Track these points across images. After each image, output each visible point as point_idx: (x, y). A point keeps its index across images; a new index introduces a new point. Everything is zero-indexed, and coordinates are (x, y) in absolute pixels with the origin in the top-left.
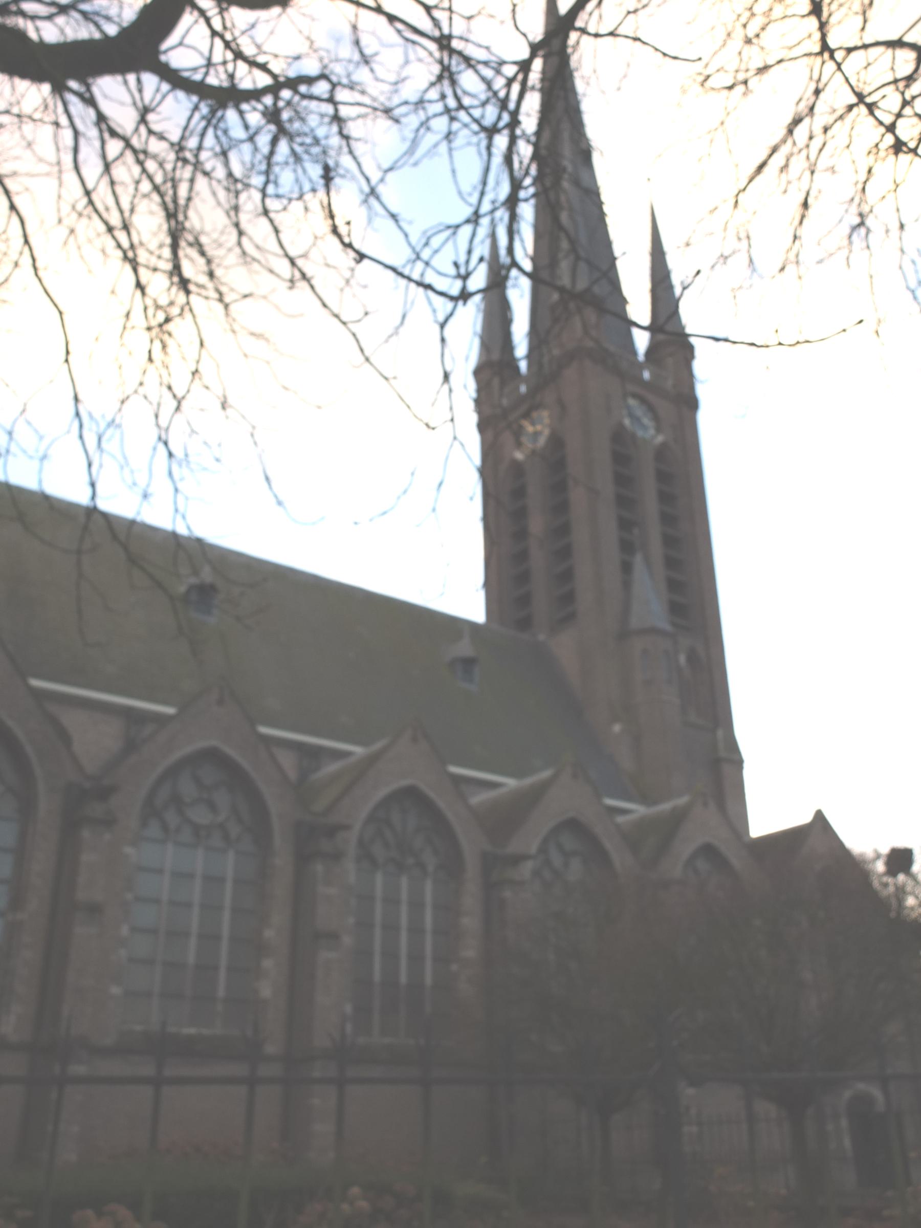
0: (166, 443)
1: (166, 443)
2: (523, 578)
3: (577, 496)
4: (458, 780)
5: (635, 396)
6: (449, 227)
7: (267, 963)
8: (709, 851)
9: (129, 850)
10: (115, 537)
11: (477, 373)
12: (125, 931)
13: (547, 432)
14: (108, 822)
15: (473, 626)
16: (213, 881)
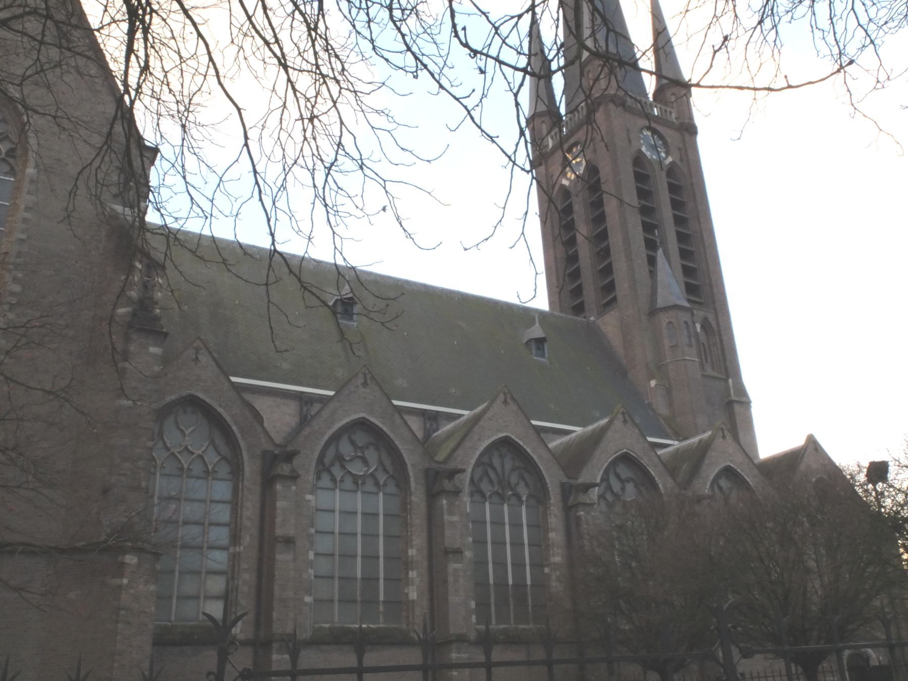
3: (611, 207)
4: (538, 430)
6: (512, 17)
7: (412, 574)
8: (729, 472)
9: (309, 497)
12: (311, 555)
14: (294, 477)
15: (541, 313)
16: (370, 516)
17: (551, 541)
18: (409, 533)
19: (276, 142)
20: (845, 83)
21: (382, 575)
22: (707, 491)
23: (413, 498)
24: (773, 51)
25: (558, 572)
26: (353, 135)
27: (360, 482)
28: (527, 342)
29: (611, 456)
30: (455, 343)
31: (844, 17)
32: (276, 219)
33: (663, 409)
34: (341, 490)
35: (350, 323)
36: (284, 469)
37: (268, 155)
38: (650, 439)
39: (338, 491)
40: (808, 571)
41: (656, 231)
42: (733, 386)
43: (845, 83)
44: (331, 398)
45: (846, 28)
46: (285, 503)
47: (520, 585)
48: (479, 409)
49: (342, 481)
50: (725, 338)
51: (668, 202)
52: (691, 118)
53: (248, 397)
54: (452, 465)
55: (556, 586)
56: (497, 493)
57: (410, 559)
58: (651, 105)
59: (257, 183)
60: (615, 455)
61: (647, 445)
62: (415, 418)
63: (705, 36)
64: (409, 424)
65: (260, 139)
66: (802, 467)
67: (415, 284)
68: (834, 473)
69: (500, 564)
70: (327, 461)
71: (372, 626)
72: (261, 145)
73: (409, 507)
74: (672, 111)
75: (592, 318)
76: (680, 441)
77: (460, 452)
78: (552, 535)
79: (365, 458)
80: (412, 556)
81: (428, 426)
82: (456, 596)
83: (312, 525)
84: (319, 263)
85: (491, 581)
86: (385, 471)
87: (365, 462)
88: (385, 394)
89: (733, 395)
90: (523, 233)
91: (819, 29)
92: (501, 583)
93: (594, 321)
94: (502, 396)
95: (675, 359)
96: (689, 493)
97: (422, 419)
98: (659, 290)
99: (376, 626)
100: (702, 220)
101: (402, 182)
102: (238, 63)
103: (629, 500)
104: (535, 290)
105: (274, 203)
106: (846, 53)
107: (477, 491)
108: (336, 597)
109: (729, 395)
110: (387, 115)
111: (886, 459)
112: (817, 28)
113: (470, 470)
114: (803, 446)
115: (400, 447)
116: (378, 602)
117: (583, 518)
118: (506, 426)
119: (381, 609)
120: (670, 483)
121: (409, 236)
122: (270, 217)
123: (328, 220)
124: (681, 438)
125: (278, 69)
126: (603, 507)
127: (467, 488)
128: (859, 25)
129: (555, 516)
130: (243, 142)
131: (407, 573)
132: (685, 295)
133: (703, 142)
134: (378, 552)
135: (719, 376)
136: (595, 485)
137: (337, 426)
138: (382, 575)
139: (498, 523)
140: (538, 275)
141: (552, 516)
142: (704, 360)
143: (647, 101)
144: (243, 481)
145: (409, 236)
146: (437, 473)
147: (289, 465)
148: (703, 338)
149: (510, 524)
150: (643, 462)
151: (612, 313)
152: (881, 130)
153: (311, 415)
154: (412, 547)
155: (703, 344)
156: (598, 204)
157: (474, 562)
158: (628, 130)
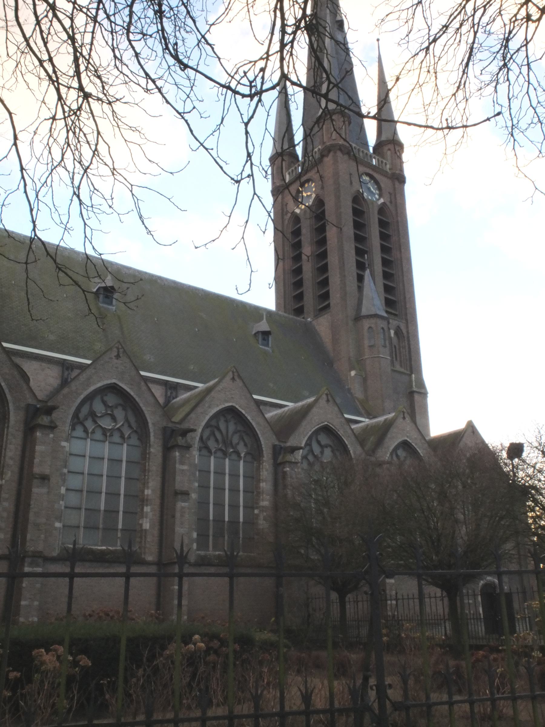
0: (78, 197)
1: (78, 197)
2: (299, 284)
3: (331, 233)
4: (258, 403)
5: (368, 175)
6: (251, 62)
7: (147, 509)
8: (406, 445)
9: (64, 444)
10: (48, 254)
11: (273, 160)
12: (63, 490)
13: (314, 196)
14: (52, 427)
15: (269, 313)
16: (115, 462)
17: (261, 490)
18: (146, 477)
19: (45, 147)
20: (514, 149)
21: (121, 509)
22: (387, 457)
23: (152, 450)
24: (462, 116)
25: (265, 514)
26: (108, 145)
27: (108, 434)
28: (255, 334)
29: (314, 427)
30: (197, 330)
31: (520, 97)
32: (38, 209)
33: (358, 393)
34: (91, 440)
35: (110, 307)
36: (45, 420)
37: (38, 157)
38: (346, 416)
39: (89, 440)
40: (457, 521)
41: (366, 255)
42: (415, 380)
43: (514, 149)
44: (89, 366)
45: (520, 107)
46: (44, 447)
47: (234, 522)
48: (212, 383)
49: (93, 432)
50: (412, 342)
51: (377, 234)
52: (402, 170)
53: (18, 360)
54: (185, 426)
55: (263, 524)
56: (221, 450)
57: (146, 497)
58: (371, 156)
59: (23, 177)
60: (318, 426)
61: (343, 420)
62: (159, 387)
63: (409, 98)
64: (153, 391)
65: (32, 142)
66: (461, 445)
67: (167, 280)
68: (483, 448)
69: (219, 505)
70: (81, 416)
71: (110, 548)
72: (32, 148)
73: (148, 456)
75: (309, 319)
76: (370, 419)
77: (193, 415)
78: (263, 485)
79: (114, 416)
80: (148, 495)
81: (169, 393)
82: (182, 528)
83: (65, 467)
84: (72, 251)
85: (211, 518)
86: (130, 426)
87: (114, 419)
88: (134, 365)
89: (414, 387)
90: (243, 238)
91: (499, 105)
92: (219, 520)
93: (311, 322)
94: (230, 375)
95: (372, 356)
96: (373, 459)
97: (164, 388)
98: (364, 302)
99: (114, 548)
100: (403, 250)
101: (147, 188)
102: (16, 77)
103: (325, 461)
104: (250, 284)
105: (37, 196)
106: (519, 127)
107: (204, 447)
108: (82, 524)
109: (411, 386)
110: (140, 132)
111: (522, 442)
112: (497, 103)
113: (200, 430)
114: (464, 429)
115: (144, 408)
116: (117, 530)
117: (288, 473)
118: (232, 398)
119: (119, 535)
120: (359, 449)
121: (149, 232)
122: (32, 207)
123: (81, 213)
124: (371, 417)
125: (48, 83)
126: (305, 465)
127: (196, 444)
128: (531, 106)
129: (267, 470)
130: (12, 142)
131: (143, 509)
132: (385, 307)
133: (408, 188)
134: (120, 490)
135: (405, 371)
136: (301, 448)
137: (92, 388)
138: (121, 509)
139: (220, 473)
140: (253, 272)
141: (264, 470)
142: (394, 359)
143: (368, 152)
144: (8, 427)
145: (149, 232)
146: (173, 431)
147: (49, 418)
148: (395, 341)
149: (229, 475)
151: (326, 316)
152: (536, 189)
153: (71, 378)
154: (148, 488)
155: (395, 347)
156: (321, 230)
157: (198, 502)
158: (351, 174)
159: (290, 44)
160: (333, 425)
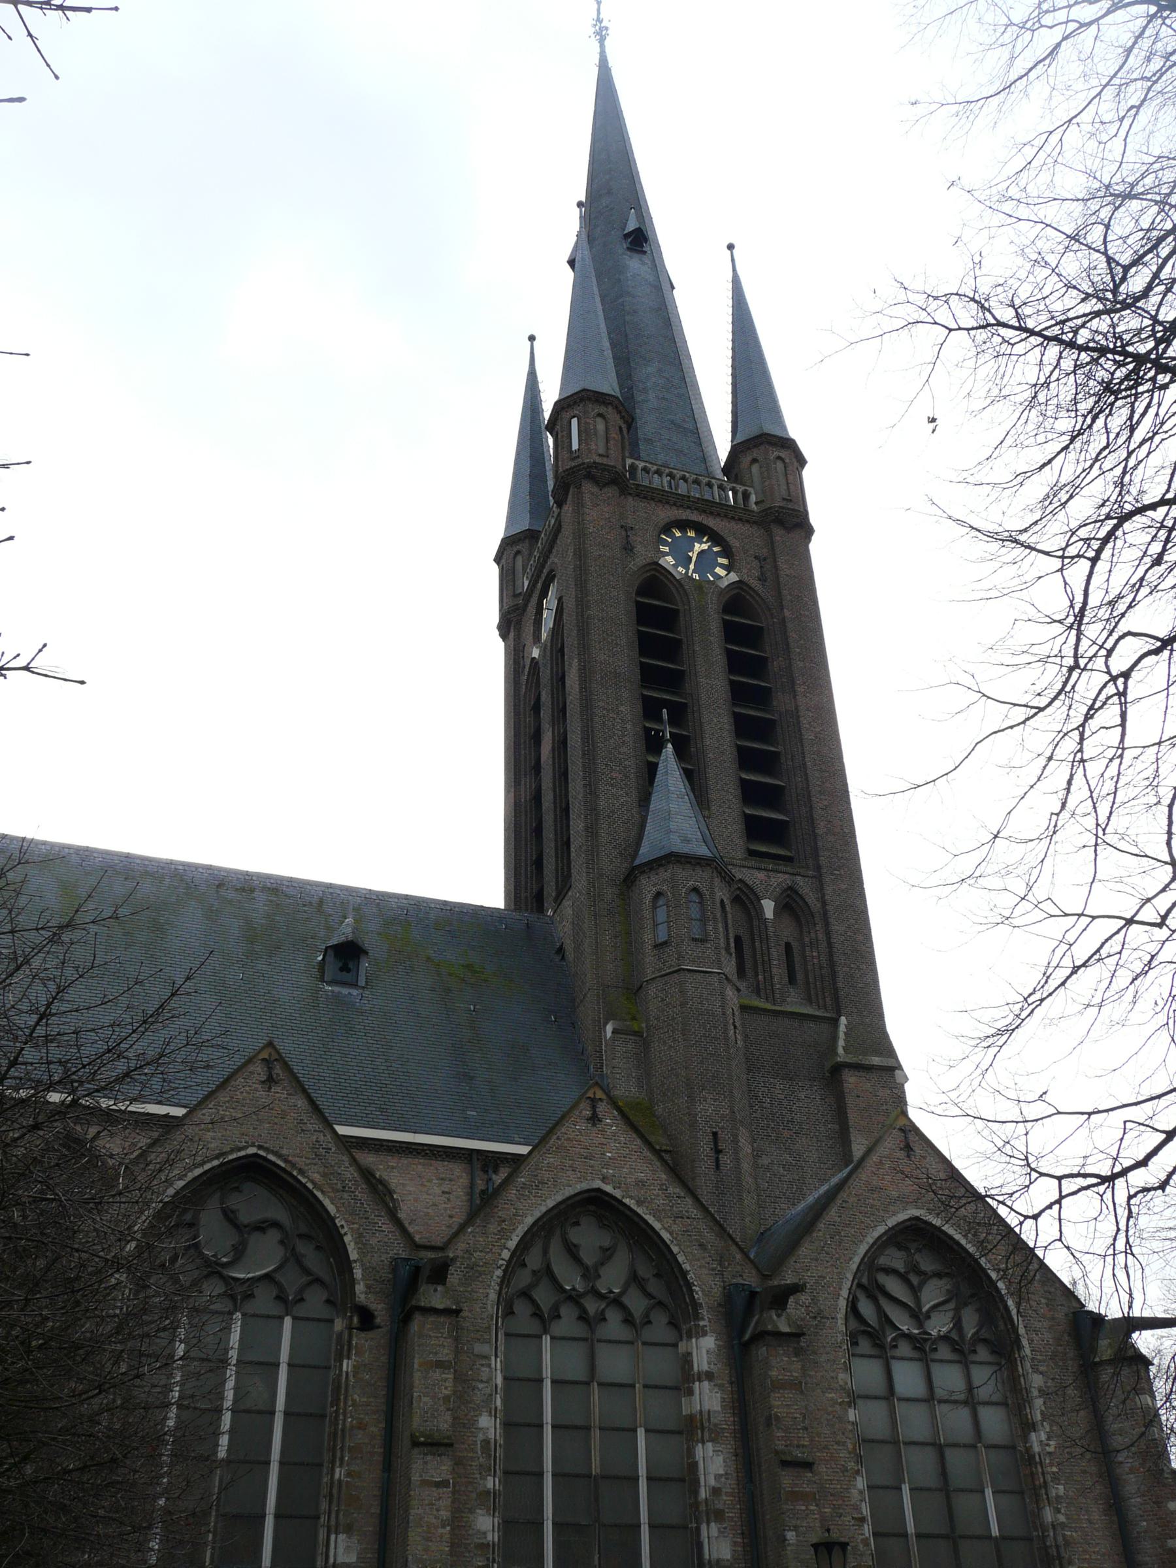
36: (435, 1298)
53: (368, 1159)
74: (750, 490)
150: (304, 1180)
159: (1115, 521)
160: (279, 1156)
